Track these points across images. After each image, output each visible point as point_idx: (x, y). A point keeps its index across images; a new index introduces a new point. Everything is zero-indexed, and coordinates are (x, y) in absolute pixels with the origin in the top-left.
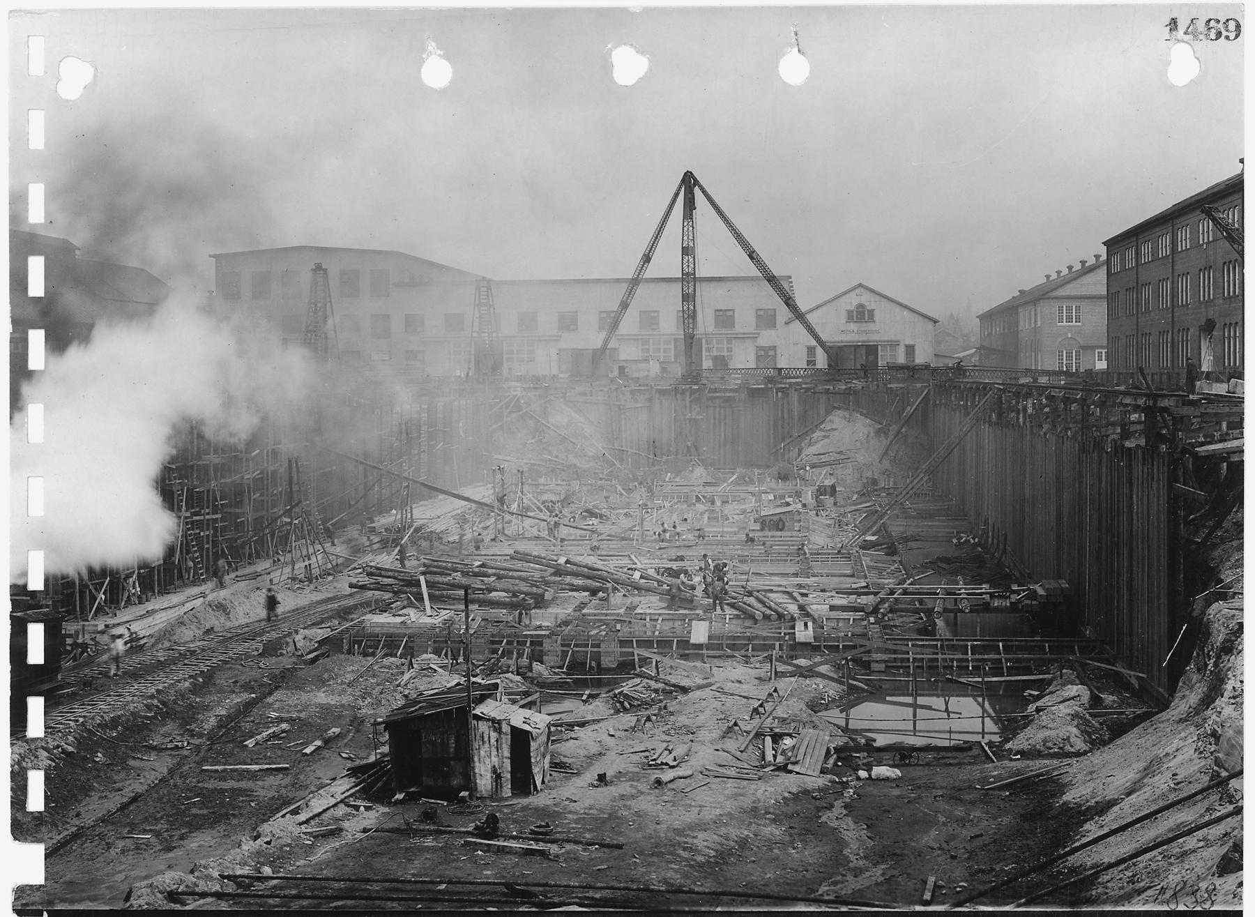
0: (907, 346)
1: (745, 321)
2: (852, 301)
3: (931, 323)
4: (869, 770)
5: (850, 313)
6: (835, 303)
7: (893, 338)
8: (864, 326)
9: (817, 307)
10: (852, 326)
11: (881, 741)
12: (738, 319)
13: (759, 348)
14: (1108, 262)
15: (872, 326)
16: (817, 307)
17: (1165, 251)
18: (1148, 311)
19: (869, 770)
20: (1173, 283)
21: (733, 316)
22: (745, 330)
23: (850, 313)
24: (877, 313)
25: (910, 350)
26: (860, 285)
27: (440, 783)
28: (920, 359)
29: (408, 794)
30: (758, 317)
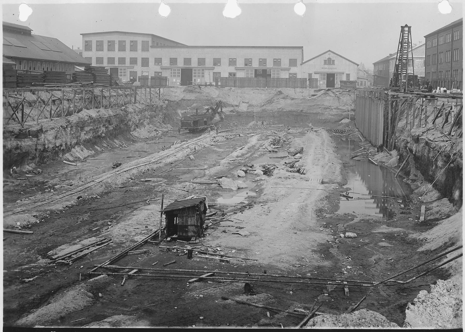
0: (347, 74)
1: (285, 63)
2: (327, 56)
3: (356, 66)
4: (344, 234)
5: (325, 61)
6: (319, 57)
7: (342, 71)
8: (331, 66)
9: (314, 58)
10: (326, 66)
11: (140, 239)
12: (207, 61)
13: (290, 74)
14: (426, 44)
15: (333, 66)
16: (314, 58)
17: (449, 40)
18: (441, 63)
19: (344, 234)
20: (452, 52)
21: (236, 61)
22: (241, 66)
23: (325, 61)
24: (336, 62)
25: (348, 75)
26: (329, 51)
27: (184, 234)
28: (352, 79)
29: (172, 238)
30: (260, 61)
